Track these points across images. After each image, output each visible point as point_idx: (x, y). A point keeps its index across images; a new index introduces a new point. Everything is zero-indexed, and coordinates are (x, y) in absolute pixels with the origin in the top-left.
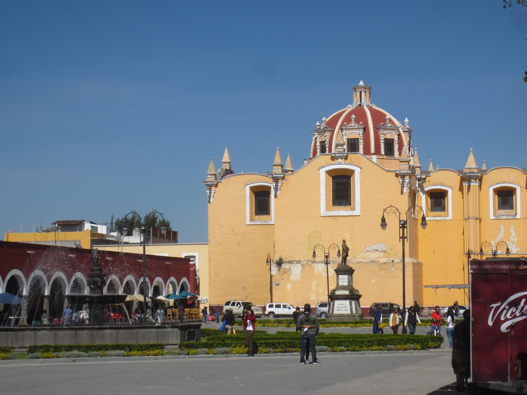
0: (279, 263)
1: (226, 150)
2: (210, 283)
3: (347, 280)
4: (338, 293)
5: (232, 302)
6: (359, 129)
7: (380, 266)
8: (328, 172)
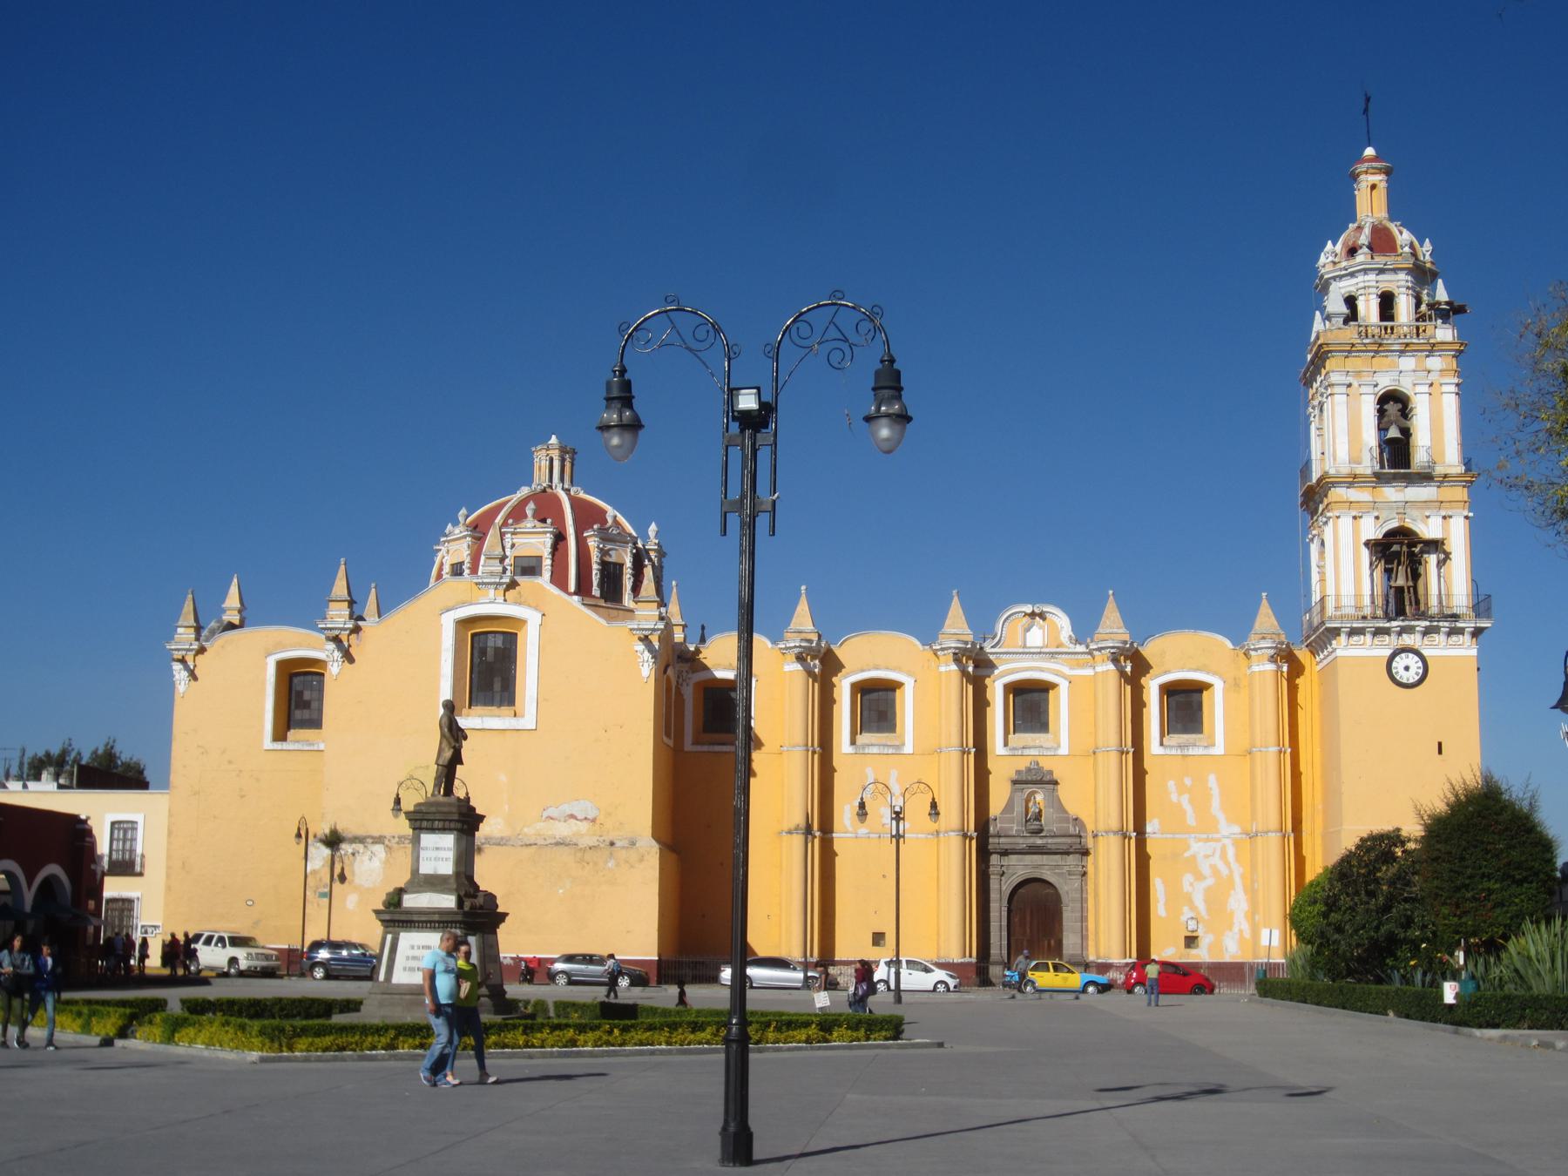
0: (333, 841)
2: (168, 888)
3: (451, 855)
7: (579, 855)
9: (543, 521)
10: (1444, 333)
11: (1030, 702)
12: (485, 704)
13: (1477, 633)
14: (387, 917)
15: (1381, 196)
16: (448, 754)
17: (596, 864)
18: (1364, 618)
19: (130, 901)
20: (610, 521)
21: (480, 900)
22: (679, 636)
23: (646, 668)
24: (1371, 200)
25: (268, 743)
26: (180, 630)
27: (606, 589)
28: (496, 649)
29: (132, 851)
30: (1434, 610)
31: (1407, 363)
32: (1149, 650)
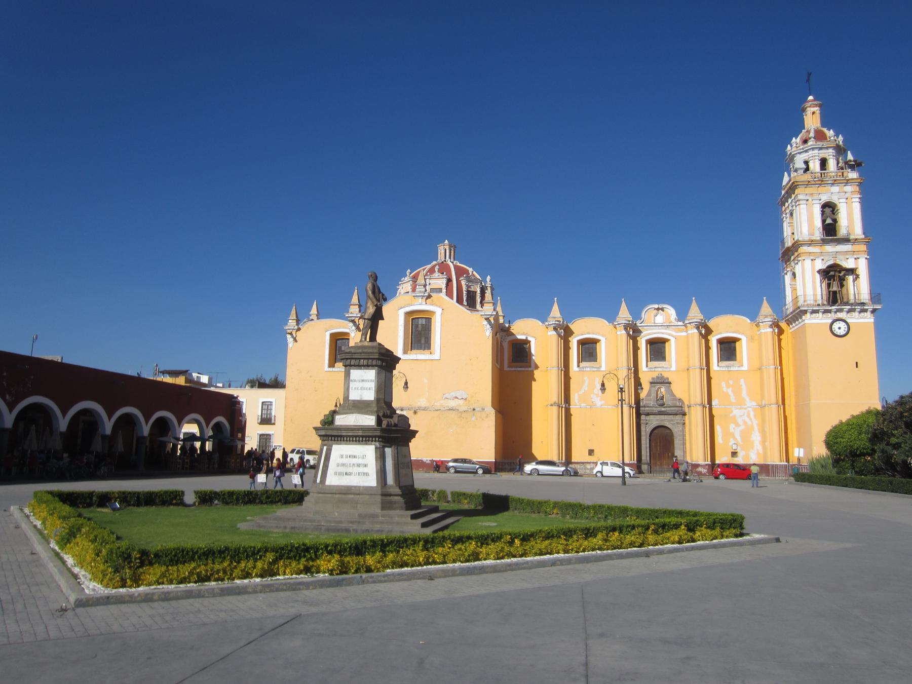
2: (285, 430)
3: (373, 385)
4: (341, 420)
10: (853, 175)
11: (657, 348)
13: (873, 311)
14: (323, 433)
15: (818, 116)
16: (371, 310)
18: (819, 305)
19: (270, 435)
21: (395, 420)
22: (501, 321)
23: (488, 332)
24: (812, 119)
25: (326, 368)
29: (270, 414)
30: (852, 301)
31: (835, 189)
32: (711, 324)
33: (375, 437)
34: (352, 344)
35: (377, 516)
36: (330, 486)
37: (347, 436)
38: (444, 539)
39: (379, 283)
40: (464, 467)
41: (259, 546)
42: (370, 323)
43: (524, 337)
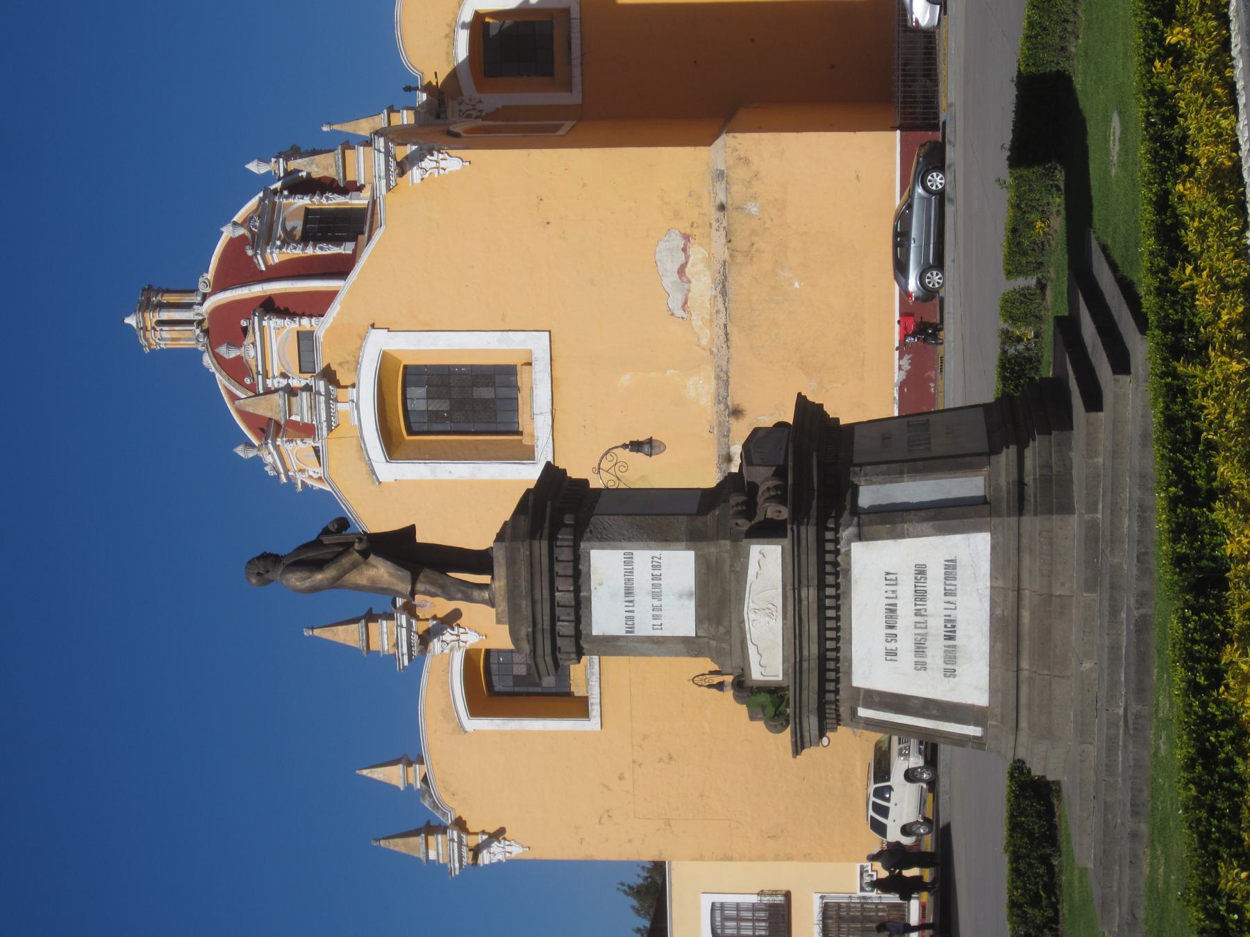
1: (365, 772)
2: (807, 857)
3: (643, 557)
4: (767, 660)
5: (871, 813)
6: (262, 328)
7: (740, 258)
8: (392, 448)
9: (245, 331)
12: (516, 410)
14: (812, 722)
16: (381, 571)
17: (753, 232)
19: (826, 908)
20: (241, 231)
21: (762, 476)
22: (406, 118)
23: (450, 163)
25: (591, 725)
26: (432, 855)
27: (341, 229)
28: (429, 397)
29: (754, 908)
33: (821, 541)
34: (501, 638)
35: (1092, 526)
36: (978, 529)
37: (822, 639)
38: (1165, 290)
39: (284, 547)
40: (921, 236)
41: (1195, 914)
42: (426, 573)
43: (463, 37)
